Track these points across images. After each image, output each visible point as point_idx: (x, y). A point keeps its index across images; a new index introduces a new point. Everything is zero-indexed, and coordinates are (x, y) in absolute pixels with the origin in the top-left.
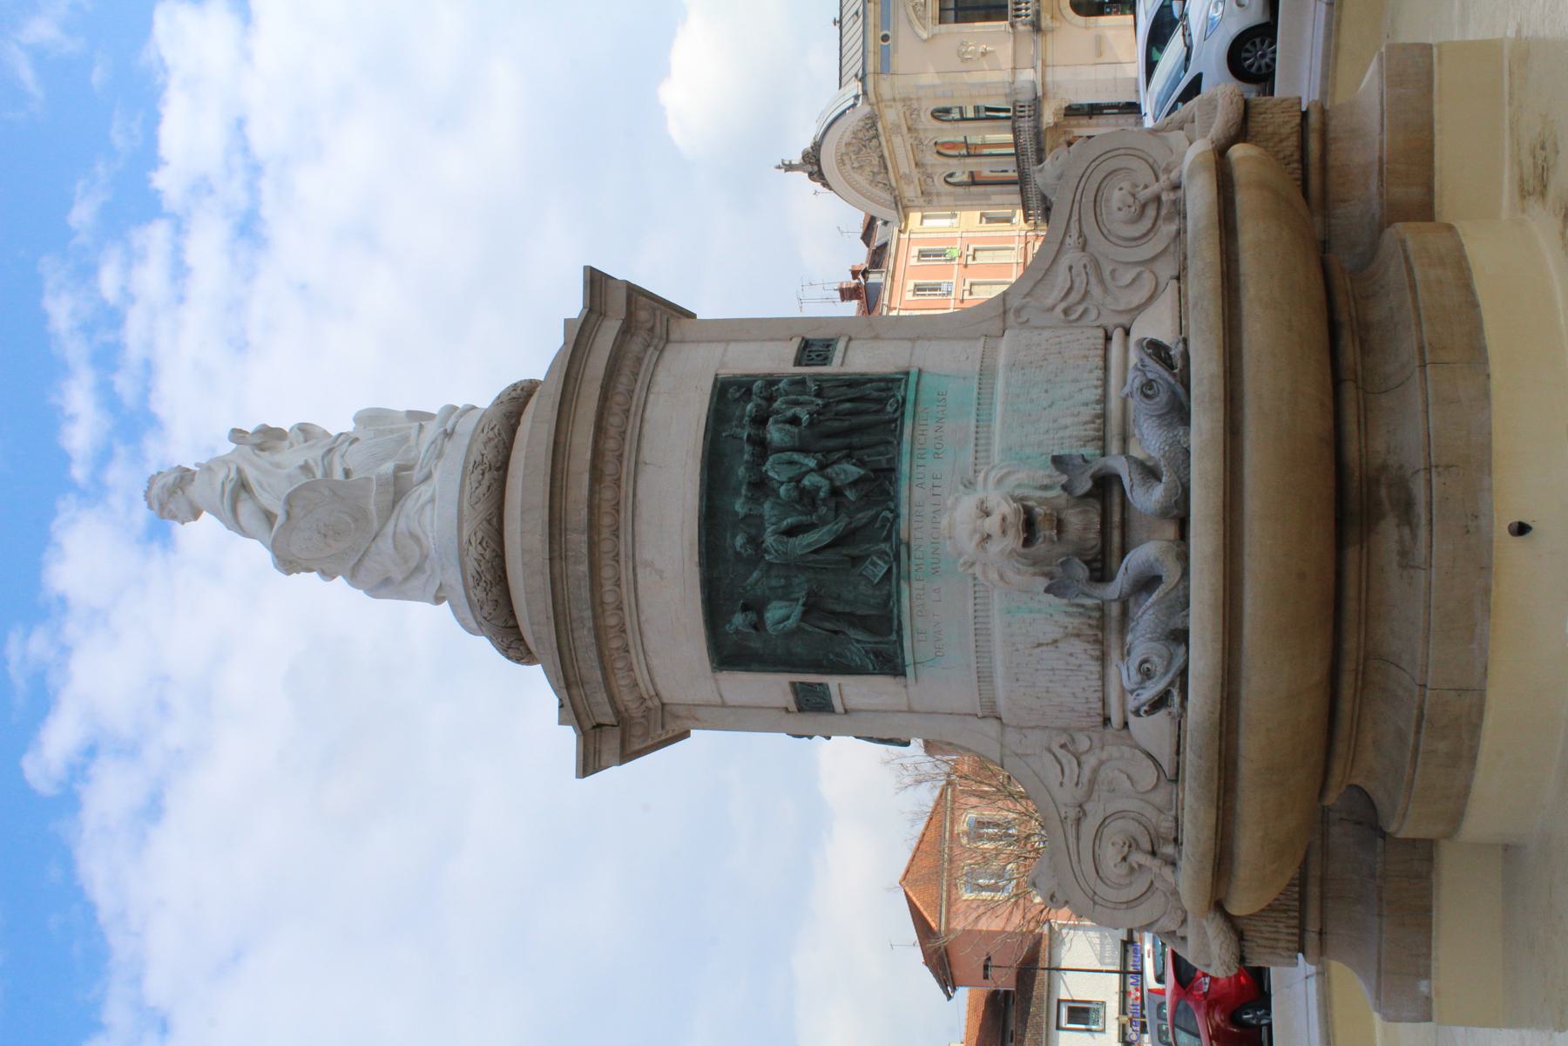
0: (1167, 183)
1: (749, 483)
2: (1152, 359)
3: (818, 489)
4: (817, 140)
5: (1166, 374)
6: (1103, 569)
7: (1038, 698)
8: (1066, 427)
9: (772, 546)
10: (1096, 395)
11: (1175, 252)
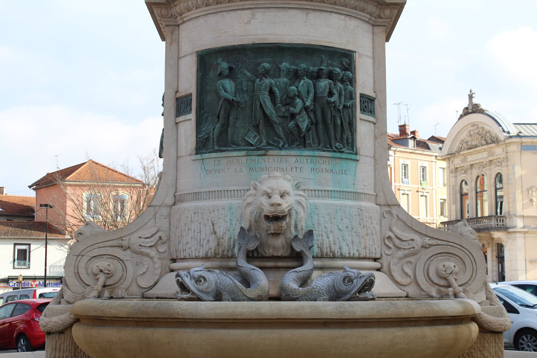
0: (458, 291)
1: (297, 70)
2: (364, 282)
3: (294, 107)
4: (486, 112)
5: (356, 289)
7: (185, 224)
8: (328, 238)
9: (264, 82)
10: (345, 253)
11: (421, 295)
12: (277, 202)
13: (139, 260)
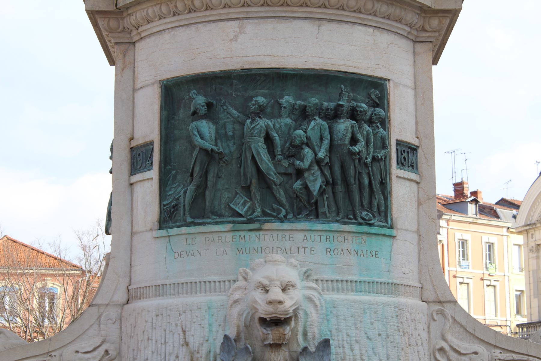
7: (144, 332)
8: (352, 350)
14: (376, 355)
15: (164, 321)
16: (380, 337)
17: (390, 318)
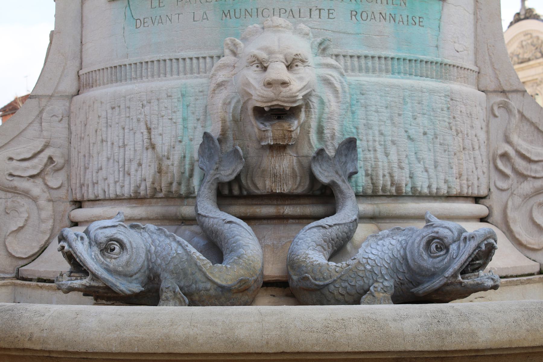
2: (475, 250)
5: (456, 266)
6: (232, 197)
7: (96, 131)
8: (387, 155)
10: (422, 187)
12: (279, 78)
13: (9, 204)
14: (419, 162)
15: (122, 116)
16: (425, 137)
17: (439, 110)
